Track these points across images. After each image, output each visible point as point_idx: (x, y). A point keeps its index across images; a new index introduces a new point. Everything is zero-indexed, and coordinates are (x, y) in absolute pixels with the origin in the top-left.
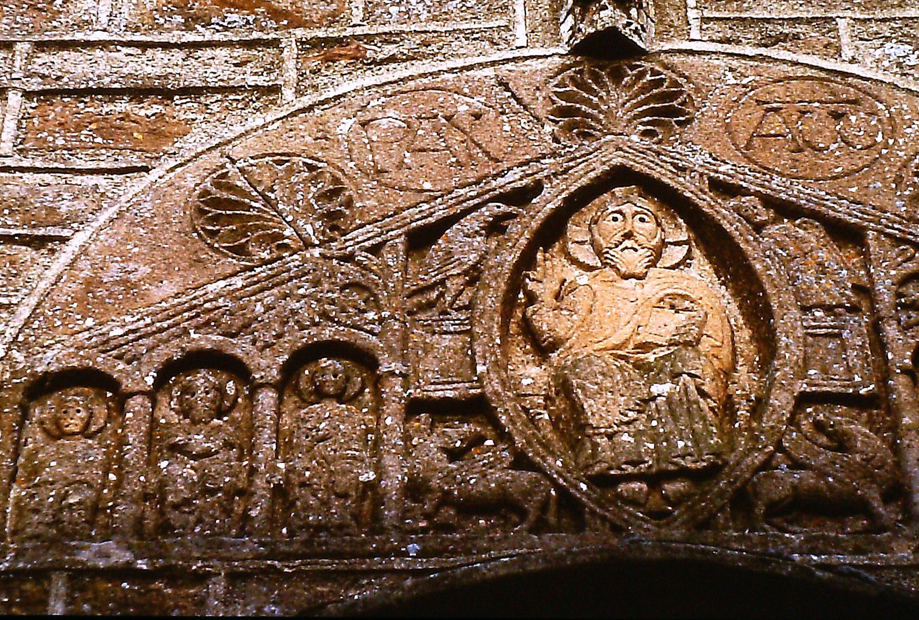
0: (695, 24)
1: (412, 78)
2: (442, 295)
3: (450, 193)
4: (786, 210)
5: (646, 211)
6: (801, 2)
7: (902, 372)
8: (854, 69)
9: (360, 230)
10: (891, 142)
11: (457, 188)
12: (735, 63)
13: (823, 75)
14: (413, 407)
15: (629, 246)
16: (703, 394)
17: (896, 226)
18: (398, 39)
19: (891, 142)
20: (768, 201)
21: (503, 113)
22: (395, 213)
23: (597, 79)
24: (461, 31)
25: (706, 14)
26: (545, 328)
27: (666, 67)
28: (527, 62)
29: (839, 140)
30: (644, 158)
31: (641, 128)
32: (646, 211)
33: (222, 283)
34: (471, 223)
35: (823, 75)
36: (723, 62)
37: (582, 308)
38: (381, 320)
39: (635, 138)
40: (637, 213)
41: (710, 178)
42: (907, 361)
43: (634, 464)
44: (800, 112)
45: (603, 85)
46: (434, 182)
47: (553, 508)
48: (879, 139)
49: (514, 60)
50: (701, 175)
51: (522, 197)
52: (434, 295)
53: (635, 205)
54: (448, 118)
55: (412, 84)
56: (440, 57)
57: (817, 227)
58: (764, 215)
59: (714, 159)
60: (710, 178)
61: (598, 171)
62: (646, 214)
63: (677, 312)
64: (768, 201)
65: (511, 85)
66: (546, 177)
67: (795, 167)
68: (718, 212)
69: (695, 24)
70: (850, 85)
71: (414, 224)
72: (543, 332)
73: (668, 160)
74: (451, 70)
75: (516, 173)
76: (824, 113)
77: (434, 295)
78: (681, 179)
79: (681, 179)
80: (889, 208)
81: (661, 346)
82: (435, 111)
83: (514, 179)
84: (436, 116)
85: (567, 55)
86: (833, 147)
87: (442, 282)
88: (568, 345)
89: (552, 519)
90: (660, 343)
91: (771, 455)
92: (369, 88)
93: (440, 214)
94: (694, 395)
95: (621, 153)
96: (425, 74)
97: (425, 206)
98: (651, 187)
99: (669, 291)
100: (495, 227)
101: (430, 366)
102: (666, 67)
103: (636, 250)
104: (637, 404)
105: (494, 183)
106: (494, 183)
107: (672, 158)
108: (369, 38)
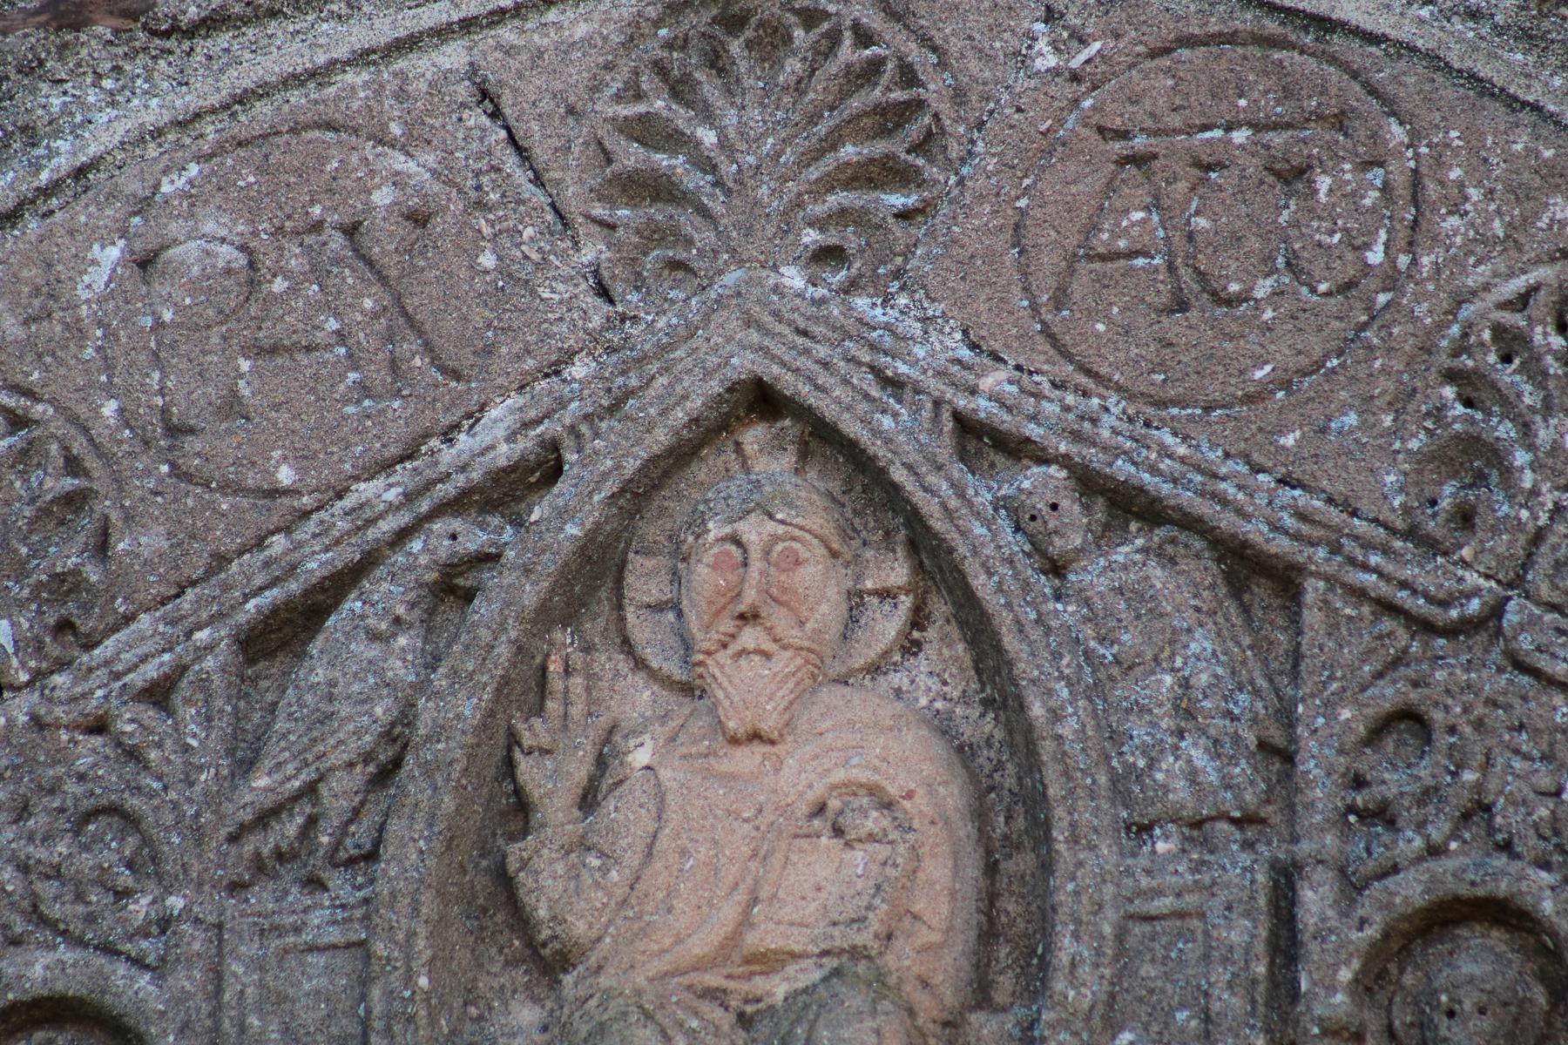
1: (262, 91)
2: (312, 821)
4: (1126, 507)
5: (797, 532)
9: (121, 636)
11: (357, 479)
15: (751, 646)
17: (1375, 559)
20: (1088, 482)
21: (480, 205)
22: (209, 573)
23: (716, 62)
29: (1280, 261)
31: (811, 236)
32: (797, 532)
34: (387, 593)
38: (165, 923)
39: (793, 278)
40: (776, 539)
41: (958, 416)
42: (1339, 998)
46: (303, 459)
50: (937, 404)
52: (291, 827)
54: (351, 231)
57: (1198, 556)
58: (1073, 525)
59: (973, 346)
60: (958, 416)
61: (695, 404)
62: (794, 539)
63: (848, 845)
64: (1088, 482)
65: (506, 100)
66: (573, 429)
67: (1161, 366)
70: (1333, 60)
72: (540, 922)
74: (362, 58)
75: (501, 416)
76: (1253, 167)
77: (291, 827)
78: (887, 422)
80: (1364, 506)
81: (803, 956)
82: (316, 211)
83: (495, 438)
84: (317, 227)
86: (1263, 288)
88: (593, 960)
90: (797, 948)
92: (157, 133)
93: (315, 566)
95: (755, 337)
97: (279, 543)
98: (821, 439)
99: (840, 775)
103: (767, 655)
105: (448, 456)
106: (448, 456)
107: (873, 347)
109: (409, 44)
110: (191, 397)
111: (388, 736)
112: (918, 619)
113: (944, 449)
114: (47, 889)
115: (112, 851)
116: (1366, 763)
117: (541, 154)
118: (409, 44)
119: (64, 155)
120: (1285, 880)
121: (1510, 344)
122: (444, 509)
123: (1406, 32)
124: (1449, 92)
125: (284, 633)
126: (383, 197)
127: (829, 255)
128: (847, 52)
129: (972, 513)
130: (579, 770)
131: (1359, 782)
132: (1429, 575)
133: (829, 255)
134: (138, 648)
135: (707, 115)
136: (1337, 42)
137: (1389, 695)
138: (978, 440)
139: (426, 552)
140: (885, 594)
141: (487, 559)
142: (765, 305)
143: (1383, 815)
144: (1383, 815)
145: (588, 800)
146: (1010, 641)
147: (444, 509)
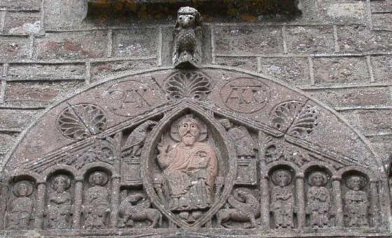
0: (214, 58)
1: (125, 77)
4: (235, 124)
8: (261, 75)
12: (225, 72)
13: (251, 77)
14: (122, 188)
16: (206, 184)
20: (231, 121)
23: (182, 77)
25: (217, 55)
27: (204, 73)
33: (66, 147)
35: (251, 77)
47: (161, 221)
49: (158, 70)
51: (157, 118)
52: (129, 151)
54: (136, 91)
55: (126, 79)
58: (229, 125)
64: (231, 121)
74: (138, 74)
83: (155, 112)
87: (132, 147)
91: (225, 204)
93: (133, 124)
98: (196, 115)
100: (149, 129)
102: (204, 73)
106: (149, 114)
108: (113, 62)
109: (144, 73)
110: (115, 105)
111: (142, 142)
112: (207, 137)
113: (213, 115)
114: (98, 156)
115: (106, 152)
116: (268, 151)
117: (160, 85)
118: (144, 73)
119: (101, 82)
120: (258, 164)
121: (283, 109)
122: (148, 119)
123: (268, 78)
124: (274, 84)
125: (127, 132)
126: (141, 87)
127: (196, 97)
128: (198, 77)
129: (217, 124)
130: (166, 148)
131: (267, 153)
132: (276, 132)
133: (196, 97)
134: (108, 132)
135: (180, 81)
136: (259, 79)
137: (271, 143)
138: (217, 116)
139: (147, 123)
140: (204, 133)
141: (154, 125)
142: (189, 101)
143: (270, 156)
144: (270, 156)
145: (167, 152)
146: (222, 136)
147: (148, 119)
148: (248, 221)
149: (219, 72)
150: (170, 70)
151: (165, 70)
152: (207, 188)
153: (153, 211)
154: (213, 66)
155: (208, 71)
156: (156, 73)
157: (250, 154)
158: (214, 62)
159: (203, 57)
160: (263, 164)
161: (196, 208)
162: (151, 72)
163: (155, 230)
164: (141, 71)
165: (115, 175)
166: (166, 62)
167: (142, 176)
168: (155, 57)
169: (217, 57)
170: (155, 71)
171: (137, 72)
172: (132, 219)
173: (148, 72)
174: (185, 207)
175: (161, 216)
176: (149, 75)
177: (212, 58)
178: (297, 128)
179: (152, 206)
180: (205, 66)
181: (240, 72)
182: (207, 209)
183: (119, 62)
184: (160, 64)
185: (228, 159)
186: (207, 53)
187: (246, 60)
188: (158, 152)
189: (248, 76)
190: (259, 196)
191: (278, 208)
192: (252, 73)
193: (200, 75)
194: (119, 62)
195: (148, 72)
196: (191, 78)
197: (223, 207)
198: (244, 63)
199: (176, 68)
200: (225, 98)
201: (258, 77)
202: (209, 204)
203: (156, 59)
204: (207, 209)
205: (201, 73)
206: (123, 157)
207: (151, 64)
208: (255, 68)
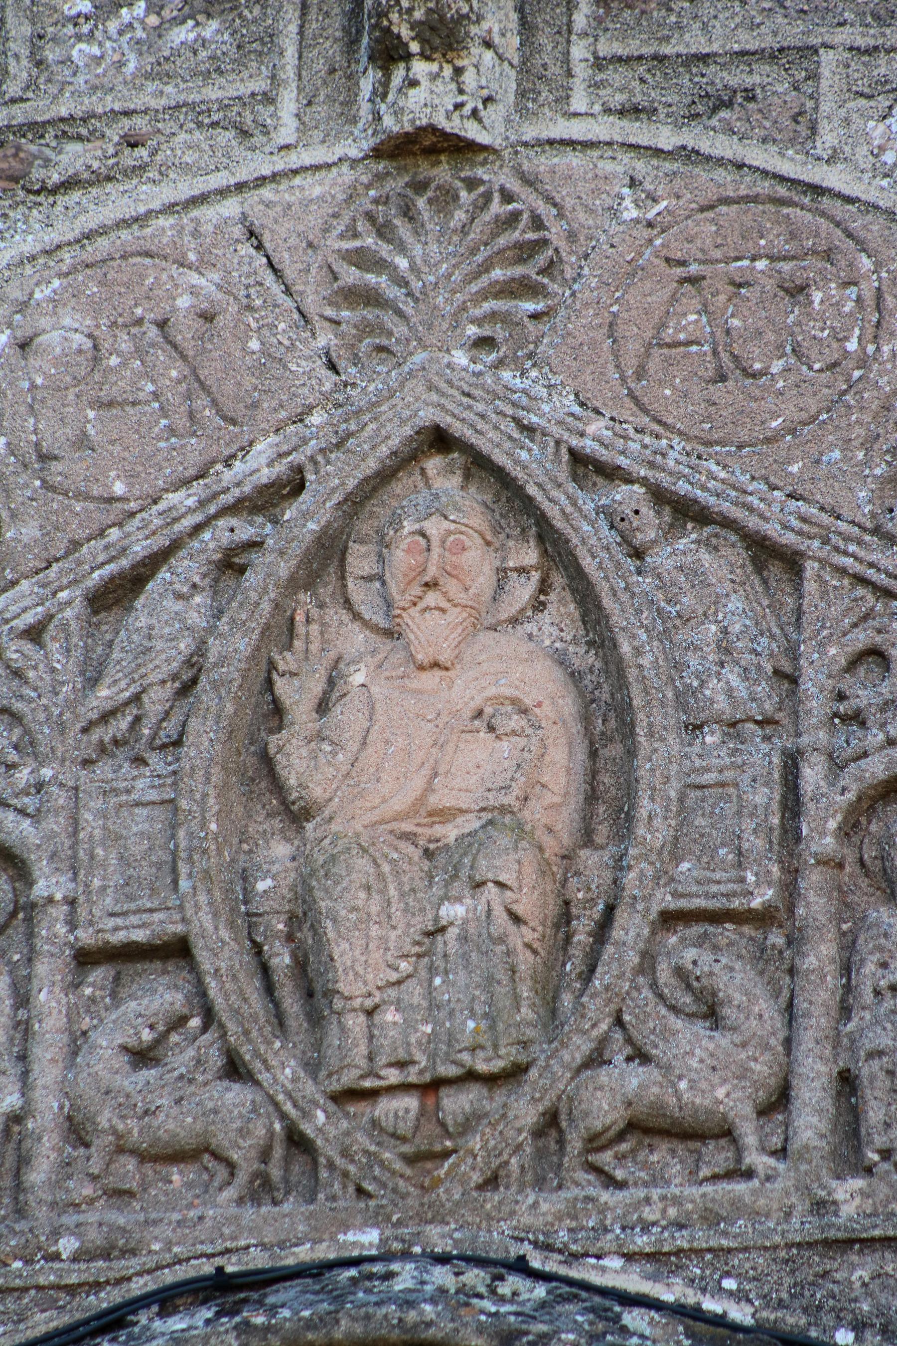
0: (581, 71)
1: (102, 231)
2: (137, 719)
3: (155, 502)
4: (685, 512)
5: (463, 528)
6: (767, 5)
7: (818, 863)
8: (833, 178)
10: (871, 349)
11: (167, 491)
12: (641, 167)
13: (782, 191)
14: (85, 959)
15: (433, 605)
16: (516, 919)
17: (852, 548)
18: (84, 132)
19: (871, 349)
20: (659, 496)
21: (249, 308)
22: (68, 553)
23: (408, 212)
24: (192, 106)
25: (605, 48)
26: (293, 782)
27: (529, 181)
28: (297, 181)
29: (788, 349)
30: (470, 407)
31: (472, 330)
32: (463, 528)
34: (187, 567)
35: (782, 191)
36: (621, 165)
37: (351, 739)
38: (40, 786)
39: (461, 358)
40: (449, 533)
41: (572, 451)
43: (401, 1065)
44: (733, 283)
45: (418, 230)
46: (131, 477)
47: (278, 1152)
48: (852, 345)
49: (275, 177)
50: (558, 443)
51: (271, 498)
53: (446, 518)
54: (162, 324)
55: (103, 244)
56: (152, 174)
58: (649, 524)
59: (582, 404)
60: (572, 451)
64: (659, 496)
66: (312, 459)
67: (709, 418)
68: (575, 530)
69: (581, 71)
70: (823, 214)
71: (96, 575)
73: (509, 411)
74: (170, 209)
75: (264, 448)
78: (524, 455)
79: (524, 455)
83: (259, 465)
84: (139, 322)
85: (363, 159)
87: (136, 698)
89: (276, 1173)
90: (464, 807)
91: (603, 1041)
94: (500, 916)
95: (434, 397)
96: (124, 221)
97: (114, 534)
98: (479, 466)
100: (231, 564)
101: (105, 879)
102: (529, 181)
103: (443, 610)
104: (418, 943)
105: (228, 476)
106: (228, 476)
107: (514, 404)
108: (36, 129)
112: (544, 587)
116: (847, 683)
117: (290, 273)
120: (792, 764)
123: (871, 196)
125: (118, 593)
127: (485, 343)
128: (496, 207)
131: (841, 697)
136: (826, 202)
137: (861, 638)
138: (585, 467)
140: (522, 570)
141: (254, 545)
142: (442, 376)
143: (857, 718)
144: (857, 718)
146: (607, 602)
148: (726, 1133)
149: (607, 166)
150: (347, 174)
151: (316, 168)
152: (519, 937)
153: (236, 1095)
154: (576, 130)
155: (542, 163)
156: (267, 193)
157: (753, 709)
158: (579, 103)
159: (524, 68)
160: (812, 775)
161: (452, 1071)
162: (240, 187)
163: (249, 1213)
164: (185, 189)
165: (48, 884)
166: (321, 110)
167: (184, 884)
168: (260, 85)
169: (599, 63)
170: (261, 181)
171: (166, 193)
172: (133, 1152)
173: (223, 193)
174: (401, 1065)
175: (277, 1126)
176: (231, 207)
177: (569, 74)
178: (489, 306)
179: (235, 1069)
180: (530, 132)
181: (720, 162)
182: (514, 1073)
183: (68, 129)
184: (287, 133)
185: (607, 617)
186: (543, 39)
187: (757, 76)
188: (277, 713)
189: (764, 187)
190: (783, 973)
191: (880, 1053)
192: (786, 168)
193: (508, 197)
194: (68, 129)
195: (223, 193)
196: (460, 216)
197: (597, 1059)
198: (750, 95)
199: (377, 153)
200: (632, 348)
201: (817, 190)
202: (525, 1044)
203: (268, 99)
204: (514, 1073)
205: (513, 185)
206: (87, 763)
207: (245, 134)
208: (804, 127)
